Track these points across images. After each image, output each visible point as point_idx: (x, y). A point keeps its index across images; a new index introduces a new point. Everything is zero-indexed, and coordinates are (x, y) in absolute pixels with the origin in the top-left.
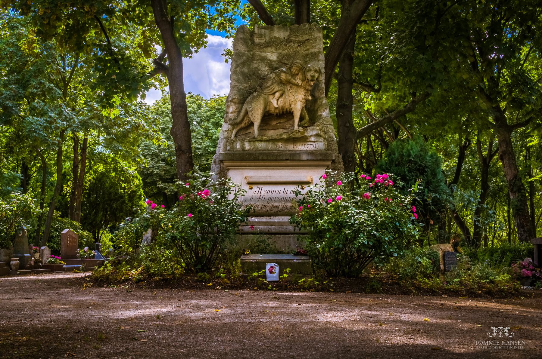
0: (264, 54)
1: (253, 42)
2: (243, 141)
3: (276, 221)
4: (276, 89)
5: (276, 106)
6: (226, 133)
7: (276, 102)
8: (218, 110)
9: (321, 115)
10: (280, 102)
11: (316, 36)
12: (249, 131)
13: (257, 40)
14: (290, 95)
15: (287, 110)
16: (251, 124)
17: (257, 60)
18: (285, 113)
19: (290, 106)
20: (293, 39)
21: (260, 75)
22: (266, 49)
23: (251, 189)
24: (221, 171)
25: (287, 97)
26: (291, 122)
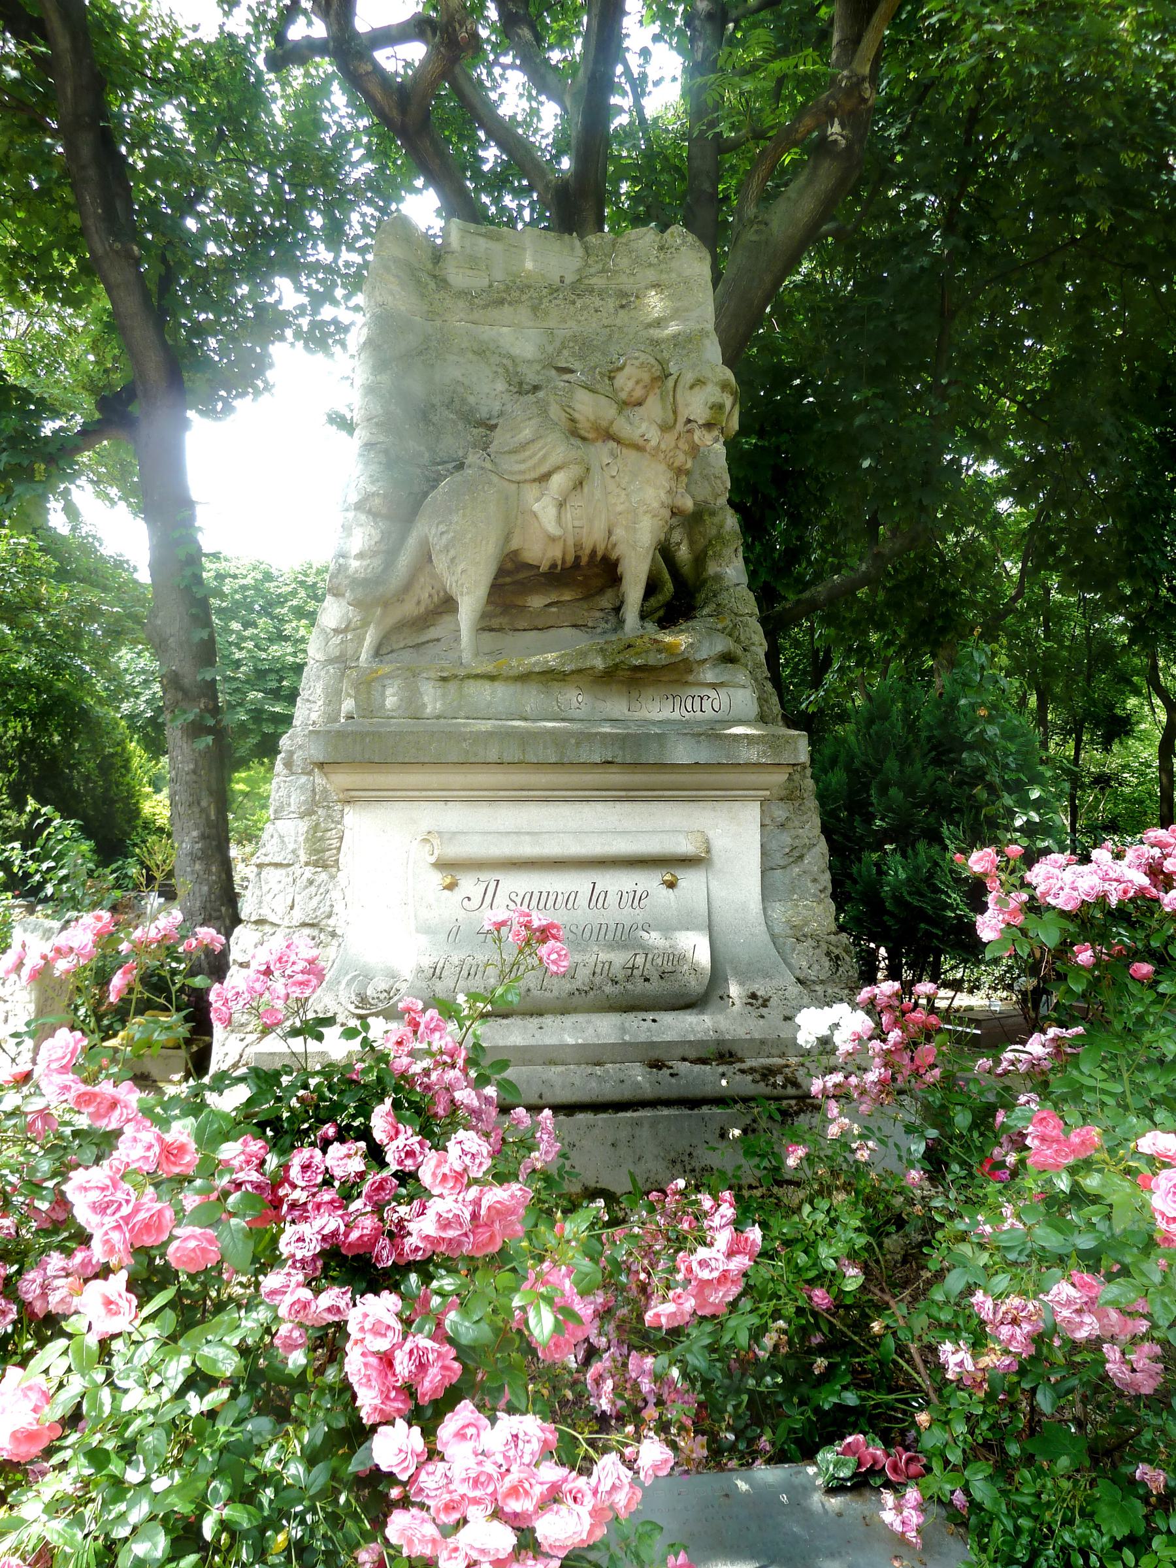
0: (487, 333)
1: (442, 283)
2: (412, 675)
3: (570, 1040)
4: (555, 458)
5: (552, 528)
6: (337, 640)
7: (552, 511)
8: (302, 583)
9: (718, 578)
10: (568, 515)
11: (688, 272)
12: (432, 633)
13: (458, 277)
14: (612, 486)
15: (594, 553)
16: (447, 605)
17: (462, 351)
18: (584, 560)
19: (610, 533)
20: (598, 282)
21: (472, 411)
22: (494, 313)
23: (451, 887)
24: (314, 803)
25: (598, 494)
26: (606, 601)
